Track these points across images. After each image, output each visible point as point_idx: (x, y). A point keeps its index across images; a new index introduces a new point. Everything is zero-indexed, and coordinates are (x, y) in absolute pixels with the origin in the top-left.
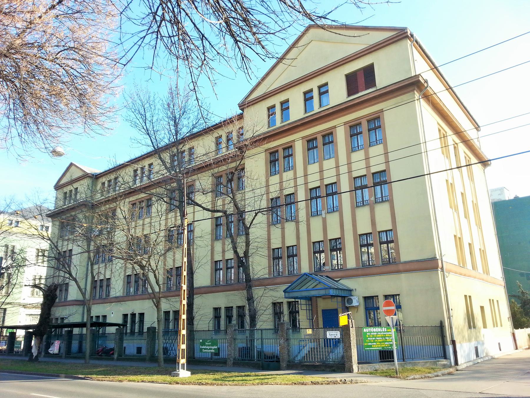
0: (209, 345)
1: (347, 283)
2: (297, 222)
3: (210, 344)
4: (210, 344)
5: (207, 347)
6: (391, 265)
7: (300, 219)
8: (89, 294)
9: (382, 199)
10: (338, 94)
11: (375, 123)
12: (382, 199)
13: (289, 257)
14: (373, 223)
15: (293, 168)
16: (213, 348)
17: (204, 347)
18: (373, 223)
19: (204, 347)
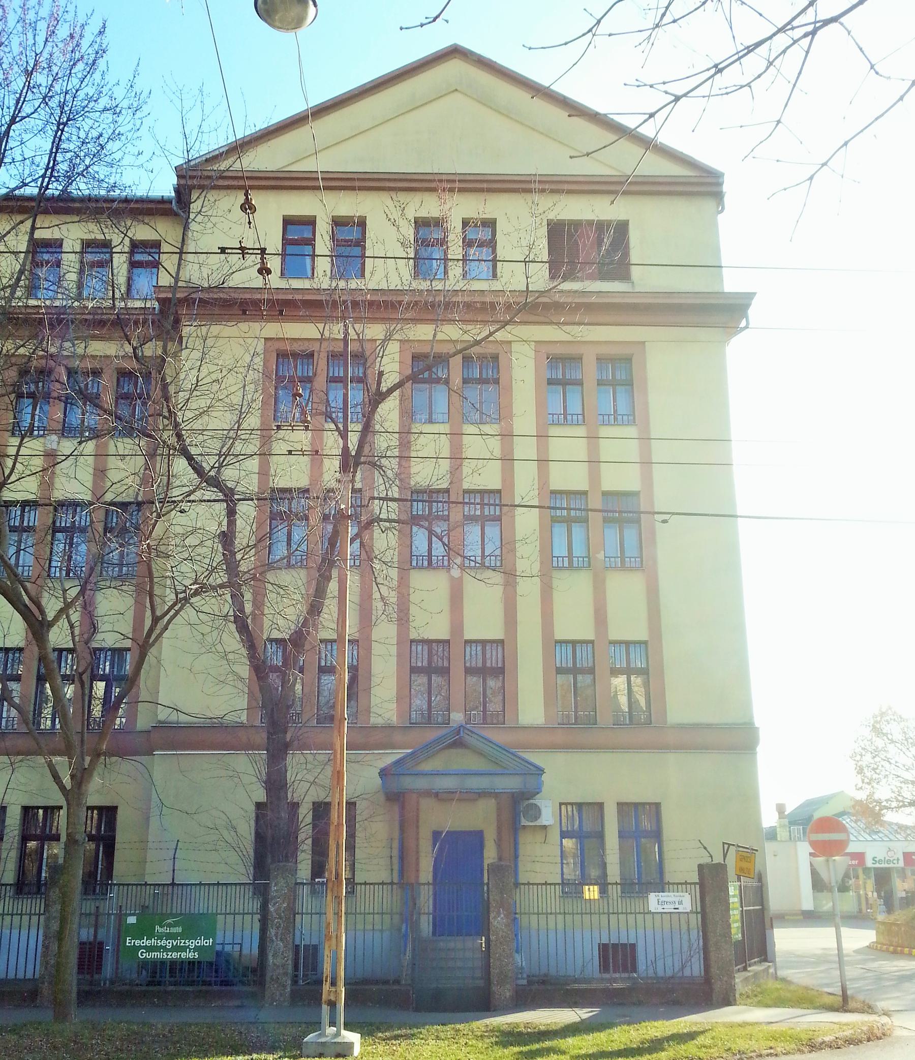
0: (170, 936)
1: (536, 758)
2: (510, 577)
3: (179, 930)
4: (179, 930)
5: (163, 943)
6: (643, 729)
7: (521, 566)
8: (422, 854)
9: (571, 562)
10: (521, 262)
11: (622, 372)
12: (571, 562)
13: (445, 672)
14: (600, 617)
15: (503, 414)
16: (192, 943)
17: (146, 942)
18: (600, 617)
19: (146, 942)
